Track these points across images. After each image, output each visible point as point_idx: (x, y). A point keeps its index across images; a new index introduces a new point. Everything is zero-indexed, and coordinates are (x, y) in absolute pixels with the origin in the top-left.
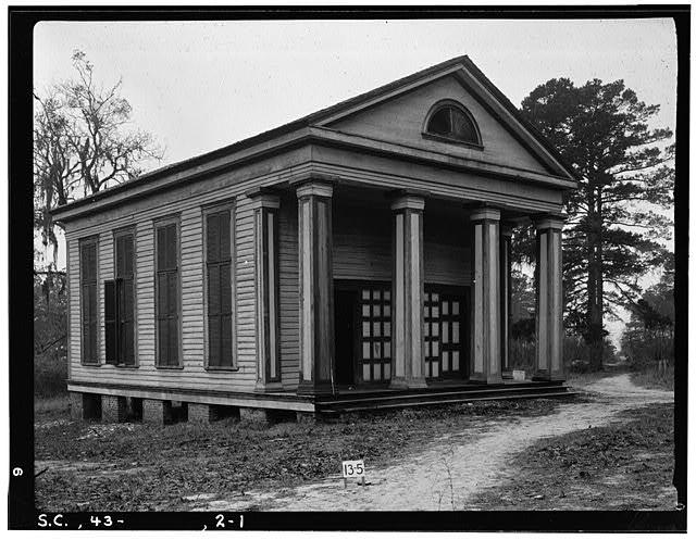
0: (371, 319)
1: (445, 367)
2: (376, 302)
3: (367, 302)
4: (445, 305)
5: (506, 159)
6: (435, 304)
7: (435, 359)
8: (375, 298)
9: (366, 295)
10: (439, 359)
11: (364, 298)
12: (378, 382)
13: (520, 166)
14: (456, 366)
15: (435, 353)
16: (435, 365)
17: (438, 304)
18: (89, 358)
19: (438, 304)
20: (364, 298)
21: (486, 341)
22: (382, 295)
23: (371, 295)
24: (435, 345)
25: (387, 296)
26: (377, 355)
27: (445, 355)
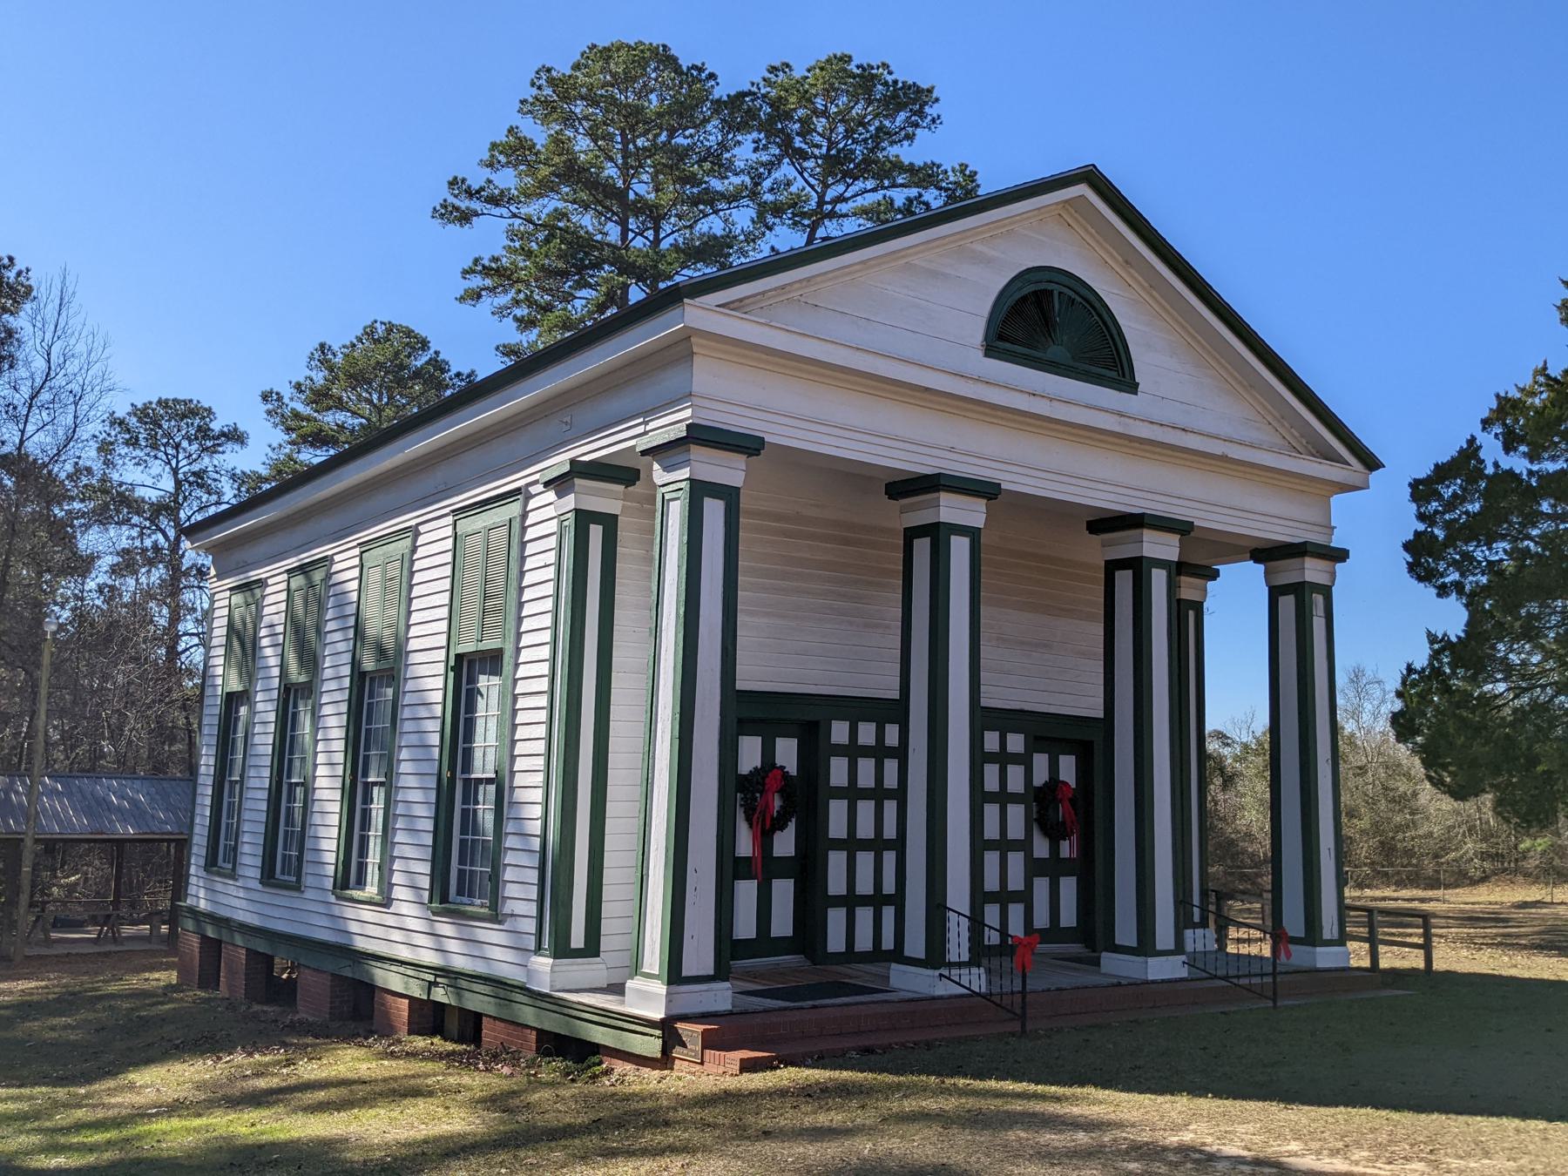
0: (853, 794)
1: (1041, 920)
2: (866, 752)
3: (839, 750)
4: (1041, 762)
5: (1283, 1115)
6: (1016, 759)
7: (1016, 897)
8: (862, 741)
9: (839, 732)
10: (1026, 897)
11: (793, 743)
12: (865, 957)
13: (1226, 430)
14: (1068, 918)
15: (1016, 882)
16: (1016, 912)
17: (1025, 760)
18: (283, 873)
19: (1025, 760)
20: (793, 743)
21: (1043, 1097)
22: (853, 733)
23: (853, 733)
24: (1016, 860)
25: (892, 735)
26: (865, 886)
27: (1041, 886)
